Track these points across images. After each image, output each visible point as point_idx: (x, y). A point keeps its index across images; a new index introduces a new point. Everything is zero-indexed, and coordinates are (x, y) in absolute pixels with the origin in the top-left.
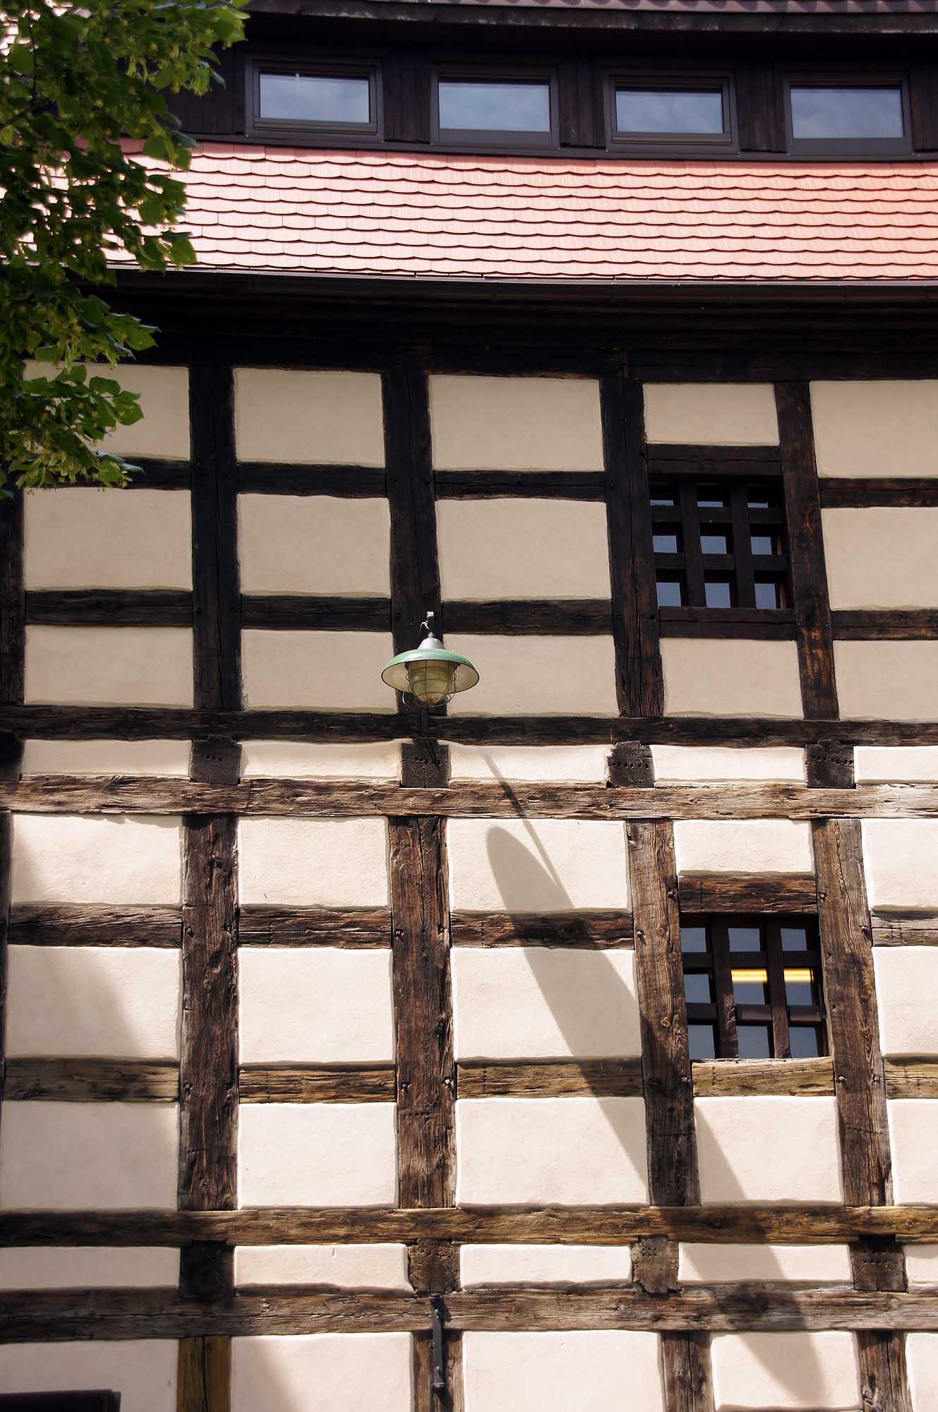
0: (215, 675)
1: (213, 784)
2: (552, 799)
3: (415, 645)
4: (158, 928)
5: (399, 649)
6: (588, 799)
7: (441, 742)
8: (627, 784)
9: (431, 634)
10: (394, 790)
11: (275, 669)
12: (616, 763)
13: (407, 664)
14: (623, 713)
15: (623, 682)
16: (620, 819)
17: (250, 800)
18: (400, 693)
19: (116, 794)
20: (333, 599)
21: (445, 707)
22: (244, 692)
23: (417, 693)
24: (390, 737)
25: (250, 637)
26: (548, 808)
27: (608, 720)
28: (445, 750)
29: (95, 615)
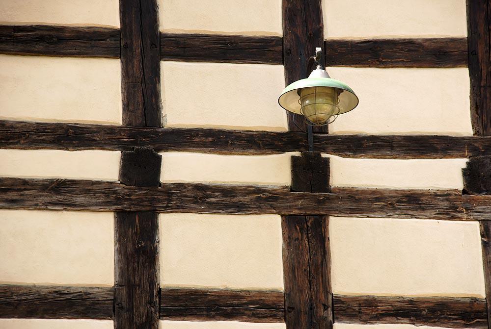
0: (140, 99)
1: (139, 185)
2: (412, 203)
3: (306, 76)
4: (94, 304)
5: (290, 80)
6: (446, 203)
7: (324, 155)
8: (479, 191)
9: (318, 67)
10: (285, 194)
11: (190, 94)
12: (468, 173)
13: (299, 91)
14: (477, 133)
15: (477, 107)
16: (475, 219)
17: (169, 201)
18: (291, 116)
19: (59, 194)
20: (235, 37)
21: (327, 127)
22: (164, 112)
23: (307, 115)
24: (281, 150)
25: (168, 68)
26: (413, 210)
27: (463, 139)
28: (327, 161)
29: (40, 47)
